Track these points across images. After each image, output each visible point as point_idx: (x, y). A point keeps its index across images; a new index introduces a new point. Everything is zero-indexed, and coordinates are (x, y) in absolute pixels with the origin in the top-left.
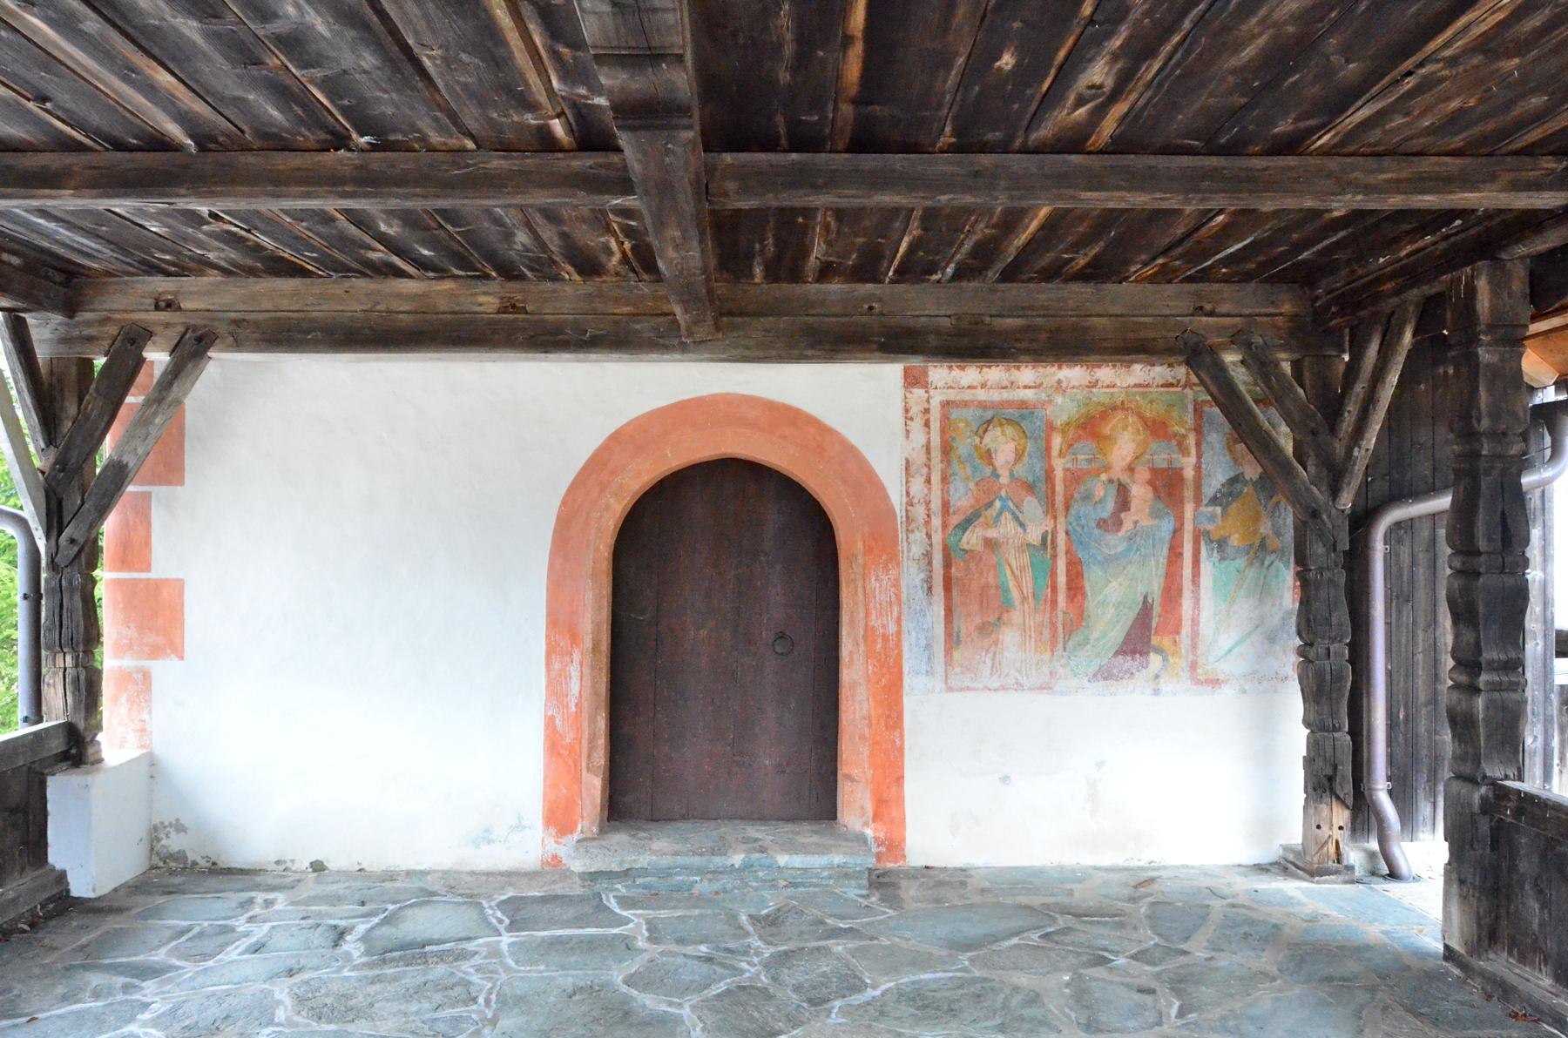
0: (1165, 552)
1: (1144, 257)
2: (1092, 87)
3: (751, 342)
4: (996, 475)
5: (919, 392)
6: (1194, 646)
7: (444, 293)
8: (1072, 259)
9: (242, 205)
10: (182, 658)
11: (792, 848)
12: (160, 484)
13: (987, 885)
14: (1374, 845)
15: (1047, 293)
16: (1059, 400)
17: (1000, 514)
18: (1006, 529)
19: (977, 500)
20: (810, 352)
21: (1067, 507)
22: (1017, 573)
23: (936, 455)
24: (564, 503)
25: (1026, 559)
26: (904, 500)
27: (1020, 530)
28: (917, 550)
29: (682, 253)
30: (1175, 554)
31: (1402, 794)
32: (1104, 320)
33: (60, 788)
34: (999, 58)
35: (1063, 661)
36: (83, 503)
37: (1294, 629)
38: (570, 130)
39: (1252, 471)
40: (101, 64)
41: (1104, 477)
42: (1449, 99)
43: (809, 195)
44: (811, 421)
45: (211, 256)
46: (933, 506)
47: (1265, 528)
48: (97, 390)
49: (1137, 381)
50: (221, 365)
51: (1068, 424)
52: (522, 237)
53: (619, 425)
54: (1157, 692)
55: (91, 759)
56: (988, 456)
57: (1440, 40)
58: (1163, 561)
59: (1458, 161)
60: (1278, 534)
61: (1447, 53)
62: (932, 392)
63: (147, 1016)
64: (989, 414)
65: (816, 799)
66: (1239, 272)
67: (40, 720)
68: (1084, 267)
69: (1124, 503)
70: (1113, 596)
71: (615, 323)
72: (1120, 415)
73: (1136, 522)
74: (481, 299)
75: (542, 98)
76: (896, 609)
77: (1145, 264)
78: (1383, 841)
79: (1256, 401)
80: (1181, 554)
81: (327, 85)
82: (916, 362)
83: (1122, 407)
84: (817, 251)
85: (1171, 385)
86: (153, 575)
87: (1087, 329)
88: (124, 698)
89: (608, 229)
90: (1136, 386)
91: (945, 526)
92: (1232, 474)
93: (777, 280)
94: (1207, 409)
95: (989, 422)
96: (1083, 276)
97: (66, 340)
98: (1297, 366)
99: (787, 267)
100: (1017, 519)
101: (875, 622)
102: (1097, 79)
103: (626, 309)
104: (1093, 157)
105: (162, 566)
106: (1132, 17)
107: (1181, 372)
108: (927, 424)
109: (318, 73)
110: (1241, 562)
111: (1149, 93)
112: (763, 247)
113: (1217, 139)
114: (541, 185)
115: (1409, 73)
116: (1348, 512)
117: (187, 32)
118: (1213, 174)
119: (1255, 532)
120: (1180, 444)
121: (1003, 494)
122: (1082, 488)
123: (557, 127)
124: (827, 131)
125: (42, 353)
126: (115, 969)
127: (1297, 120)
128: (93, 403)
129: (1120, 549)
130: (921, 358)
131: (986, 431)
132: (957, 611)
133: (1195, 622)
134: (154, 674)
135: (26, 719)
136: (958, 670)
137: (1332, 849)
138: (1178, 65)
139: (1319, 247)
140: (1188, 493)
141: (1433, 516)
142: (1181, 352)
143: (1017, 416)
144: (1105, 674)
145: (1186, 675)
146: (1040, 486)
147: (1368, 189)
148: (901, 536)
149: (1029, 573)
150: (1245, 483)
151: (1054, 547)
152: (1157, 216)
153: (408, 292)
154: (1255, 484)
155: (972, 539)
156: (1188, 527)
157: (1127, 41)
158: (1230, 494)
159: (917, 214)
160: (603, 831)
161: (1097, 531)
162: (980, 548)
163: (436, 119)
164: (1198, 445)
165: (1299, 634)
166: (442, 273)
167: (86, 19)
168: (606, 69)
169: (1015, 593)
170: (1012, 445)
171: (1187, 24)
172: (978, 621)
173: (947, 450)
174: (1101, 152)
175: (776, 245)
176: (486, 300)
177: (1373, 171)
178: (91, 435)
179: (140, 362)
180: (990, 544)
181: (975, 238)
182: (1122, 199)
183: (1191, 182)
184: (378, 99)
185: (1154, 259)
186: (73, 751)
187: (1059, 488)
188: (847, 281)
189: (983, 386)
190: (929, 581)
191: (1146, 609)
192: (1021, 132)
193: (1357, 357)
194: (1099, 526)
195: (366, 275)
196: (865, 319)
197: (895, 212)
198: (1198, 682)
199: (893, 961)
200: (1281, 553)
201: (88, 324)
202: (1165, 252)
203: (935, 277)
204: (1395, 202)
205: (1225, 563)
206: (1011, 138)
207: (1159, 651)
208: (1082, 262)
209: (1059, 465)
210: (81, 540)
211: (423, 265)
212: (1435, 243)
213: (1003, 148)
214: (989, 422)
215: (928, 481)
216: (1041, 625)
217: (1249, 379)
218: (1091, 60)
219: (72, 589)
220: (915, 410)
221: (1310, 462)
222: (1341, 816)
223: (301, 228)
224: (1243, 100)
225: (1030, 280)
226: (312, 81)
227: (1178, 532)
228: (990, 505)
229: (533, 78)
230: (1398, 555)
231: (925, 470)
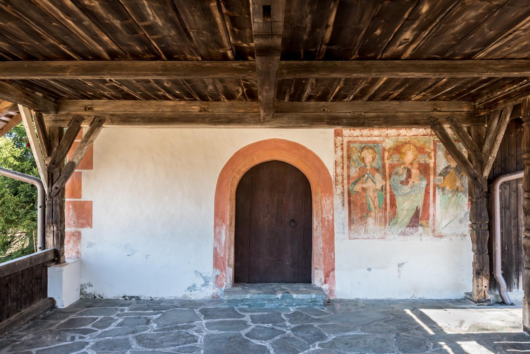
0: (424, 192)
1: (417, 93)
2: (405, 39)
3: (284, 122)
4: (365, 166)
5: (339, 138)
6: (434, 224)
7: (182, 106)
8: (393, 94)
9: (118, 78)
10: (91, 228)
11: (298, 292)
12: (85, 169)
13: (364, 305)
14: (497, 293)
15: (384, 104)
16: (387, 140)
18: (370, 184)
20: (304, 125)
22: (373, 199)
23: (345, 159)
24: (220, 175)
26: (335, 174)
27: (374, 185)
28: (339, 191)
29: (266, 94)
31: (507, 276)
32: (403, 114)
33: (52, 270)
34: (376, 31)
35: (389, 229)
36: (60, 175)
37: (468, 218)
38: (233, 53)
39: (454, 164)
40: (86, 34)
41: (402, 166)
42: (523, 42)
43: (310, 74)
44: (303, 148)
45: (106, 93)
47: (458, 184)
48: (65, 137)
49: (414, 134)
50: (107, 130)
51: (390, 149)
52: (211, 87)
53: (238, 150)
54: (421, 240)
55: (62, 261)
56: (363, 160)
57: (521, 24)
58: (423, 195)
59: (526, 61)
60: (462, 186)
61: (523, 28)
62: (344, 138)
63: (88, 346)
64: (363, 145)
65: (305, 277)
66: (451, 97)
67: (45, 249)
68: (397, 96)
69: (409, 175)
70: (406, 206)
71: (239, 115)
72: (408, 145)
74: (194, 107)
75: (226, 44)
76: (332, 212)
77: (417, 95)
78: (500, 292)
79: (455, 141)
80: (429, 193)
81: (158, 41)
82: (339, 128)
84: (308, 91)
85: (426, 135)
86: (82, 200)
87: (397, 117)
88: (72, 241)
89: (239, 85)
90: (413, 135)
91: (348, 183)
92: (447, 165)
93: (292, 101)
94: (438, 143)
95: (363, 148)
96: (395, 99)
97: (55, 121)
98: (469, 128)
99: (296, 97)
100: (373, 181)
101: (325, 216)
102: (407, 37)
103: (242, 111)
104: (404, 61)
105: (85, 197)
106: (421, 18)
107: (429, 131)
108: (342, 149)
109: (156, 37)
110: (450, 195)
111: (424, 41)
112: (290, 90)
113: (443, 55)
114: (224, 72)
115: (511, 34)
116: (487, 178)
117: (116, 24)
118: (444, 66)
119: (455, 185)
120: (428, 155)
121: (368, 172)
122: (395, 170)
123: (229, 53)
124: (317, 54)
125: (47, 125)
126: (76, 331)
127: (472, 49)
128: (64, 142)
129: (408, 191)
130: (341, 127)
131: (362, 151)
132: (352, 212)
133: (434, 216)
134: (82, 233)
135: (40, 248)
136: (353, 232)
137: (483, 294)
138: (434, 33)
139: (477, 89)
140: (432, 172)
141: (517, 181)
142: (429, 124)
143: (372, 146)
144: (404, 234)
145: (431, 234)
146: (381, 170)
147: (496, 71)
148: (334, 186)
149: (377, 200)
151: (386, 190)
152: (422, 80)
153: (169, 106)
154: (454, 169)
155: (358, 188)
156: (432, 184)
157: (418, 26)
158: (446, 172)
159: (343, 79)
160: (234, 286)
161: (400, 185)
162: (360, 191)
163: (190, 51)
164: (435, 156)
165: (471, 220)
166: (181, 98)
167: (86, 21)
168: (257, 39)
169: (372, 206)
170: (371, 156)
171: (438, 20)
172: (360, 215)
173: (349, 157)
174: (406, 59)
175: (294, 90)
176: (195, 108)
177: (497, 65)
178: (63, 153)
179: (80, 128)
180: (364, 189)
181: (361, 87)
182: (413, 75)
183: (436, 69)
184: (173, 44)
185: (421, 93)
186: (56, 259)
187: (387, 170)
188: (316, 101)
189: (361, 136)
190: (343, 202)
192: (381, 54)
193: (490, 126)
194: (401, 183)
195: (155, 99)
196: (322, 114)
197: (335, 79)
198: (436, 236)
199: (334, 329)
200: (464, 192)
201: (62, 115)
202: (425, 91)
203: (346, 100)
204: (505, 75)
205: (444, 196)
206: (377, 55)
207: (421, 225)
208: (396, 94)
209: (387, 163)
210: (60, 188)
211: (176, 96)
212: (517, 87)
213: (374, 58)
214: (363, 148)
215: (343, 168)
216: (381, 217)
217: (452, 133)
218: (406, 31)
219: (56, 204)
220: (338, 144)
221: (474, 162)
222: (485, 282)
223: (138, 85)
224: (456, 43)
225: (378, 101)
226: (153, 39)
227: (428, 185)
228: (364, 176)
229: (225, 39)
230: (504, 193)
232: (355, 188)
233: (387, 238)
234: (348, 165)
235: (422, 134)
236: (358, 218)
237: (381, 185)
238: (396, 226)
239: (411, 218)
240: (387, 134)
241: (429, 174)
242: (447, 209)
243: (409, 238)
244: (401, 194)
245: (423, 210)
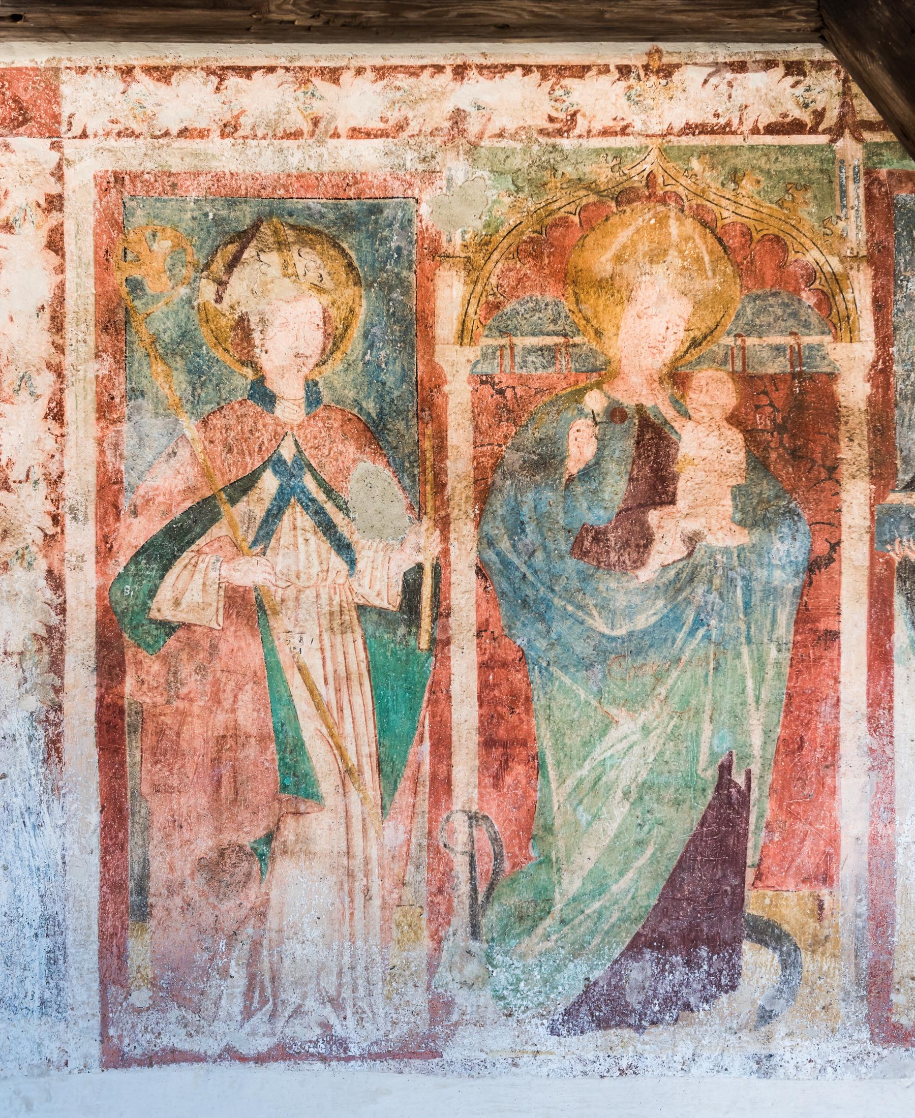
17: (274, 515)
19: (206, 473)
21: (484, 493)
22: (327, 694)
23: (81, 333)
25: (354, 652)
27: (337, 563)
30: (815, 634)
35: (472, 969)
46: (68, 488)
49: (695, 118)
51: (485, 244)
54: (764, 1065)
62: (70, 147)
73: (692, 540)
80: (833, 636)
83: (650, 192)
85: (797, 127)
90: (689, 129)
91: (105, 549)
95: (244, 238)
100: (328, 528)
108: (55, 243)
120: (826, 301)
129: (642, 622)
131: (232, 264)
140: (853, 452)
144: (603, 1009)
149: (361, 700)
150: (660, 59)
151: (441, 613)
155: (189, 591)
156: (855, 554)
161: (572, 564)
164: (880, 305)
172: (204, 844)
180: (250, 609)
189: (229, 129)
190: (51, 718)
191: (728, 806)
207: (768, 933)
209: (457, 368)
215: (57, 414)
227: (819, 565)
231: (45, 382)
232: (165, 592)
233: (452, 1053)
234: (103, 385)
235: (769, 117)
236: (185, 868)
237: (404, 561)
238: (534, 943)
239: (668, 865)
240: (458, 117)
241: (833, 470)
242: (544, 619)
243: (653, 1046)
244: (582, 648)
245: (781, 792)
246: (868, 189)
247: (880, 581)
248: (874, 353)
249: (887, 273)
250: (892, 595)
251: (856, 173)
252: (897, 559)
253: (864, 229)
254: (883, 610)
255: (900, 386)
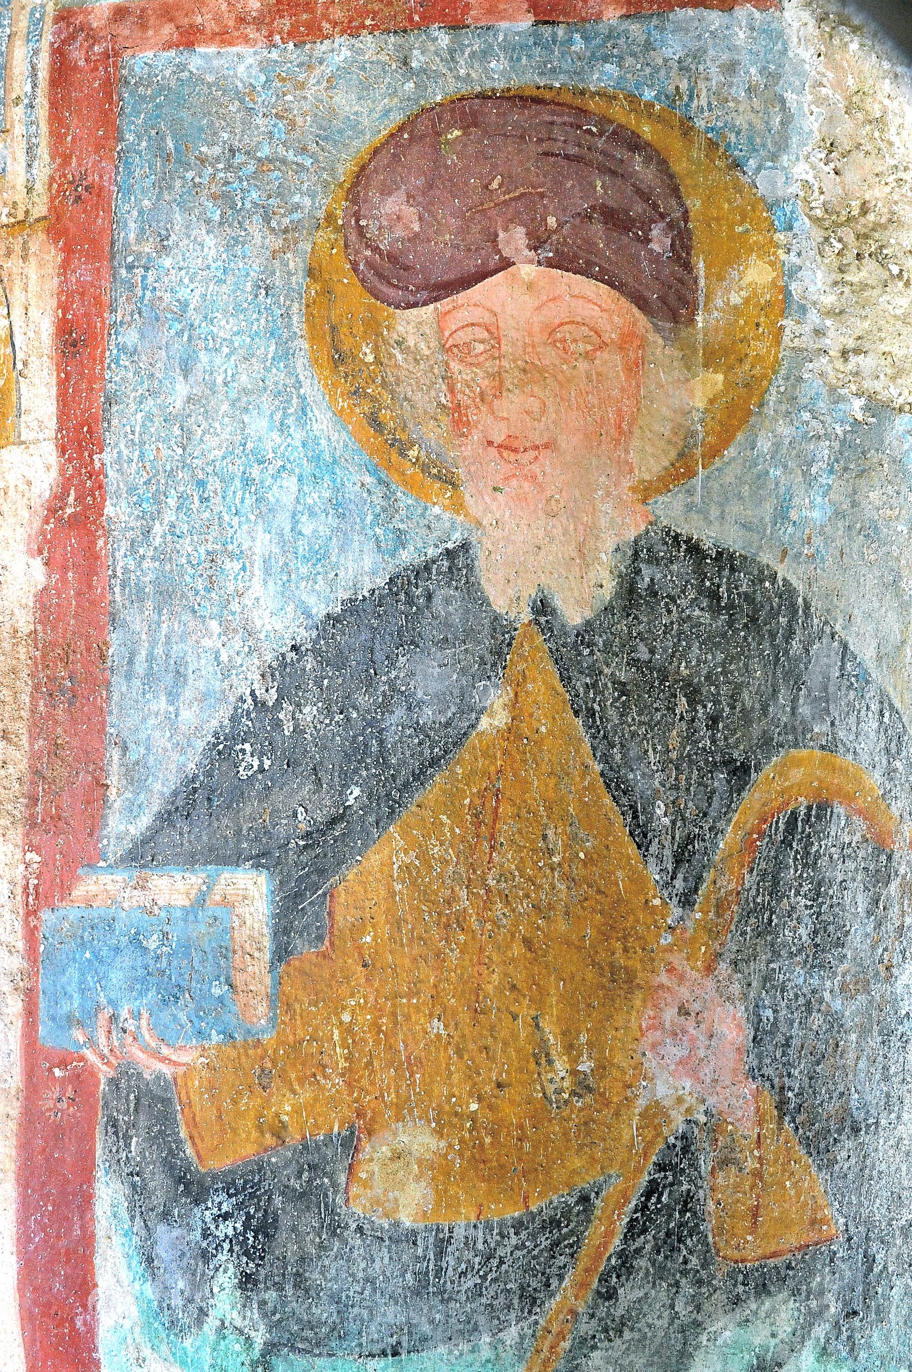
246: (59, 53)
247: (57, 1133)
248: (54, 474)
249: (94, 255)
250: (89, 1178)
251: (36, 23)
252: (104, 1073)
253: (43, 151)
254: (60, 1219)
255: (122, 561)
